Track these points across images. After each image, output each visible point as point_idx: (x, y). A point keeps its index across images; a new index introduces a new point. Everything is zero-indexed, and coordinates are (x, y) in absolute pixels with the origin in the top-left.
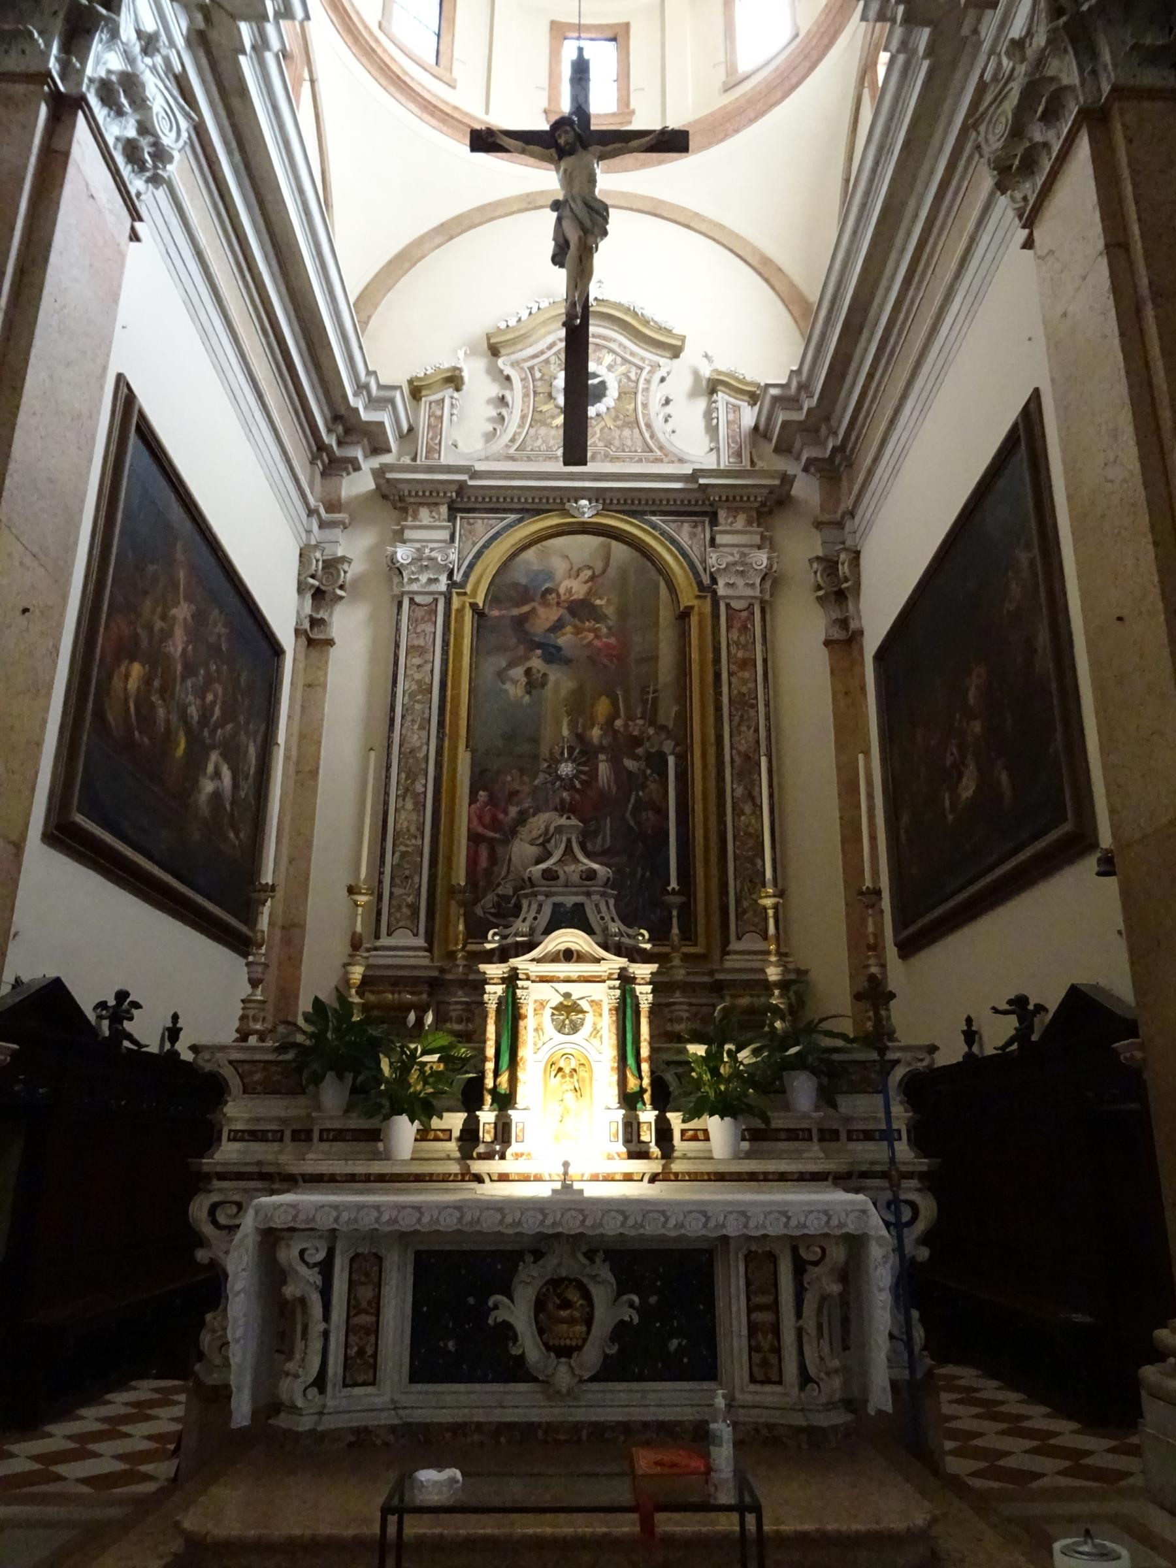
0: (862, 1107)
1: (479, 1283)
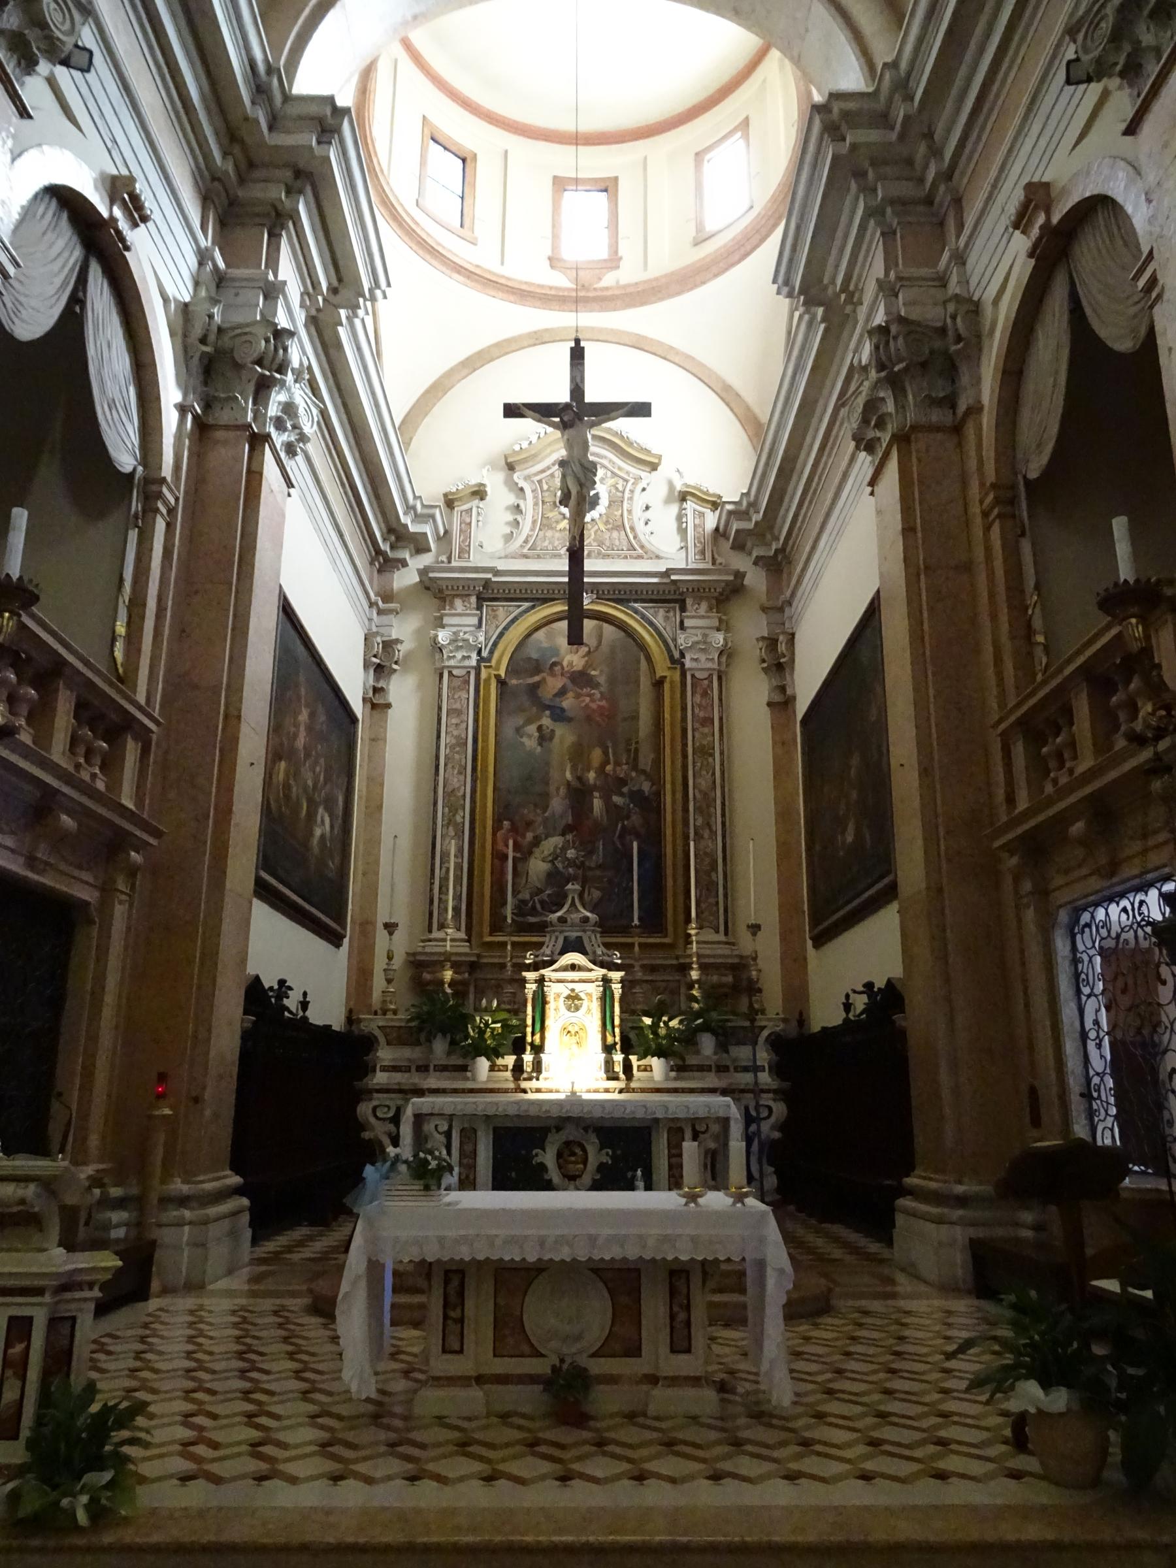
0: (742, 1053)
1: (526, 1148)
